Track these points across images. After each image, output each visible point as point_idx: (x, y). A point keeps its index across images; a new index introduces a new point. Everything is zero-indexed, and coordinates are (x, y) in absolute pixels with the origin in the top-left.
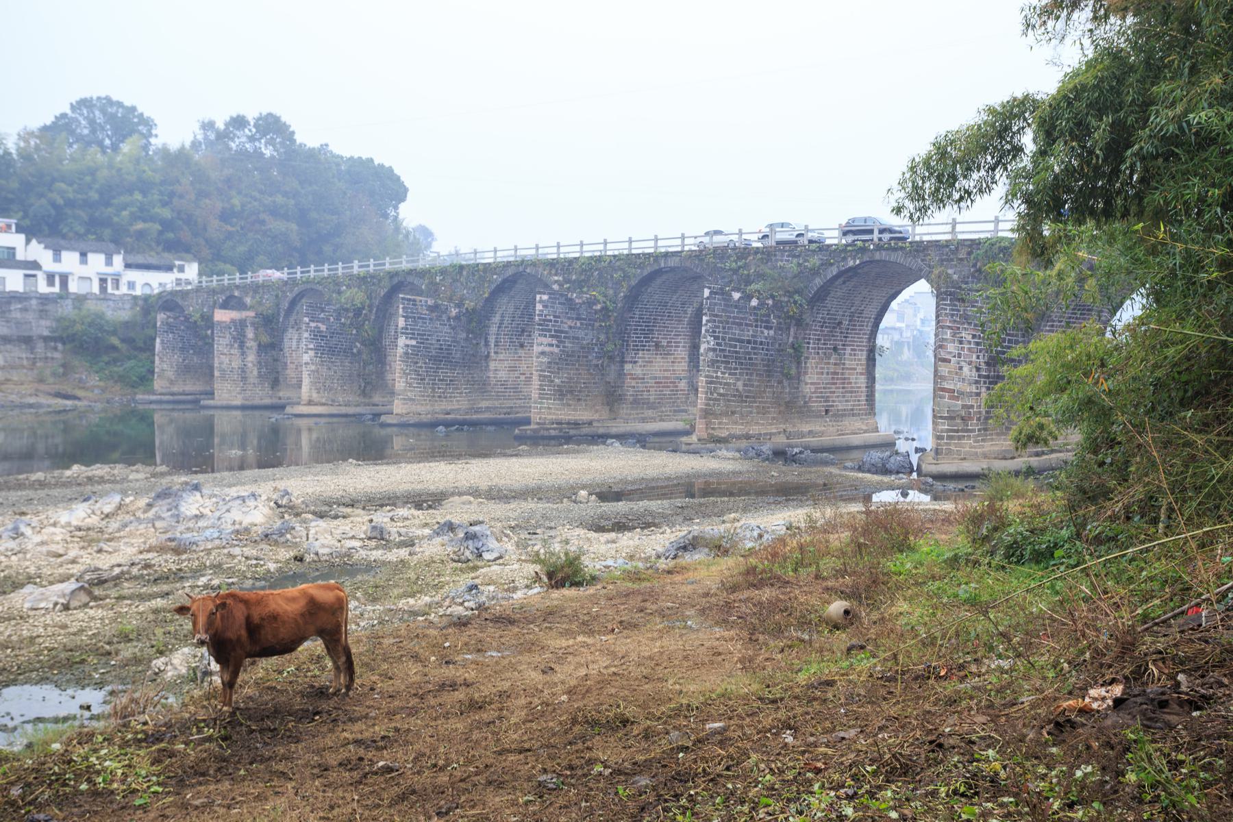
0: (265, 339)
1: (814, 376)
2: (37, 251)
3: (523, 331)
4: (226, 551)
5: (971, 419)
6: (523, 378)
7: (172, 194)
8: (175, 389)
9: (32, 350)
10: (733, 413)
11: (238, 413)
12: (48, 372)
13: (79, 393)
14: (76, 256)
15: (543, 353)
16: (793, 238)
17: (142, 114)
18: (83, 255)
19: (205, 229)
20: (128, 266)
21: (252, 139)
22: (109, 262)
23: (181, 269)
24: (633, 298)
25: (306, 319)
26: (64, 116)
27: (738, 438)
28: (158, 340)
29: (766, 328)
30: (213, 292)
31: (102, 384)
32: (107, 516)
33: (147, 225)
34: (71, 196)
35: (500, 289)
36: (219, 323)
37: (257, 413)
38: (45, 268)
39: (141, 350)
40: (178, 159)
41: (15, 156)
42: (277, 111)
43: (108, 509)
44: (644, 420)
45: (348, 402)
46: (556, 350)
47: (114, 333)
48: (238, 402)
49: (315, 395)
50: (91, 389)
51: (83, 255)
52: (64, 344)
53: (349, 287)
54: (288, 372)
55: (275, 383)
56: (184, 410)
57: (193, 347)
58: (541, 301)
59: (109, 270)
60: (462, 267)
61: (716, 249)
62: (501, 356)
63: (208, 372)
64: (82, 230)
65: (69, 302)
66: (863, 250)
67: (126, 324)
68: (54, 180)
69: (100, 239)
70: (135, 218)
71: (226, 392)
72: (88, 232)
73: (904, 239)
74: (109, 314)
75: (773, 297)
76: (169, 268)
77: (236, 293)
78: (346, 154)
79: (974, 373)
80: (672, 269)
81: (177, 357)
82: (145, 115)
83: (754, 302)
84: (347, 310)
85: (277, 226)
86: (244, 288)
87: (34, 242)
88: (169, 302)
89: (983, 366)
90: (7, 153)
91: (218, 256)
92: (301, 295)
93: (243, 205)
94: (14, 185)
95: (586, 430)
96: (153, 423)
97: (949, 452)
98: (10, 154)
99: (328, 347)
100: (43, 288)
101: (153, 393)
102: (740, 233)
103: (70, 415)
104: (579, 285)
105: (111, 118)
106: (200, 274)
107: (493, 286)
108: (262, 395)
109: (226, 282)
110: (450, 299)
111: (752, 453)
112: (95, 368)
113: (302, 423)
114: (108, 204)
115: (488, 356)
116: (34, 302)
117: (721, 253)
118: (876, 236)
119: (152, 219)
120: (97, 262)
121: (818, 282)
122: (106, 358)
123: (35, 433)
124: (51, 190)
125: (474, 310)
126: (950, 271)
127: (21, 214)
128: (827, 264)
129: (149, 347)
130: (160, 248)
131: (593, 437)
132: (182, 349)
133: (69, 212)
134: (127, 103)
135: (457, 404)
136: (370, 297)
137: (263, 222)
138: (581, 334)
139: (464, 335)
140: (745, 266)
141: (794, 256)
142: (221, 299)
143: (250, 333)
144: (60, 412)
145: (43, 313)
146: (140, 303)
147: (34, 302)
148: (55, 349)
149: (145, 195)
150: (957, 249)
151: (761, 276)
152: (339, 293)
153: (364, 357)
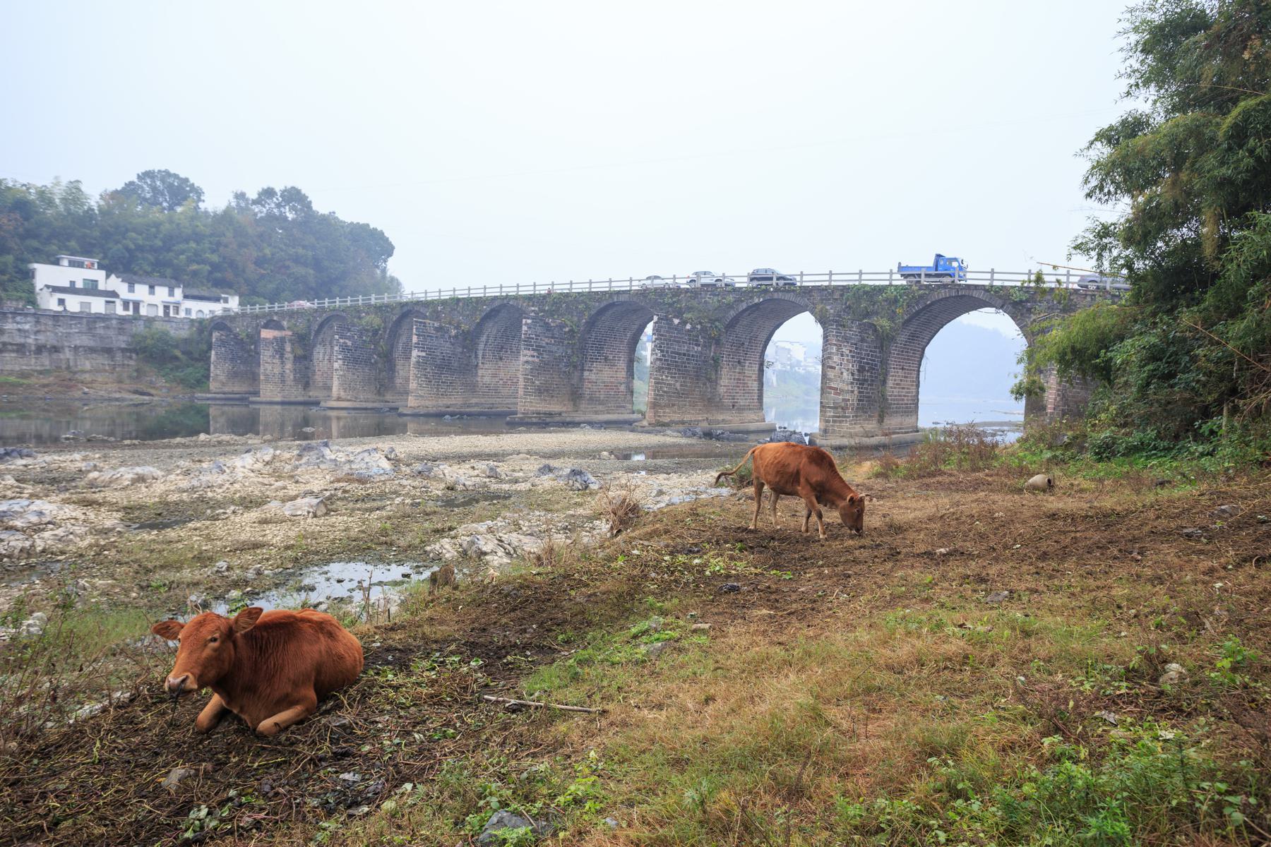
0: (300, 352)
1: (726, 380)
2: (115, 283)
3: (502, 348)
4: (397, 482)
5: (848, 409)
6: (501, 382)
7: (219, 244)
8: (226, 389)
9: (113, 358)
10: (673, 405)
11: (278, 407)
12: (125, 375)
13: (153, 391)
14: (146, 288)
15: (527, 362)
16: (713, 282)
17: (193, 184)
18: (152, 287)
19: (244, 271)
20: (186, 297)
21: (278, 206)
22: (171, 294)
23: (226, 301)
24: (592, 323)
25: (337, 337)
26: (132, 183)
27: (677, 423)
28: (213, 352)
29: (696, 345)
30: (257, 317)
31: (167, 385)
32: (267, 463)
33: (201, 266)
34: (141, 242)
35: (488, 317)
36: (265, 339)
37: (293, 408)
38: (122, 296)
39: (197, 360)
40: (225, 217)
41: (97, 212)
42: (299, 186)
43: (267, 458)
44: (596, 413)
45: (367, 398)
46: (536, 360)
47: (176, 347)
48: (278, 399)
49: (342, 394)
50: (160, 388)
51: (152, 287)
52: (137, 354)
53: (367, 313)
54: (316, 377)
55: (306, 386)
56: (232, 405)
57: (240, 358)
58: (526, 324)
59: (171, 299)
60: (459, 300)
61: (656, 289)
62: (486, 366)
63: (254, 378)
64: (149, 269)
65: (141, 323)
66: (766, 291)
67: (186, 341)
68: (127, 230)
69: (163, 276)
70: (190, 261)
71: (269, 392)
72: (153, 270)
73: (794, 284)
74: (172, 332)
75: (701, 323)
76: (217, 300)
77: (275, 318)
78: (348, 220)
79: (850, 377)
80: (622, 303)
81: (228, 366)
82: (196, 185)
83: (688, 327)
84: (367, 331)
85: (299, 270)
86: (282, 314)
87: (113, 276)
88: (219, 324)
89: (856, 372)
90: (91, 209)
91: (254, 292)
92: (328, 320)
93: (273, 255)
94: (97, 233)
95: (557, 419)
96: (208, 415)
97: (834, 431)
98: (93, 210)
99: (353, 358)
100: (120, 311)
101: (209, 392)
102: (675, 278)
103: (145, 408)
104: (551, 314)
105: (170, 187)
106: (240, 304)
107: (483, 314)
108: (296, 394)
109: (267, 310)
110: (450, 324)
111: (689, 433)
112: (162, 373)
113: (333, 414)
114: (169, 250)
115: (477, 366)
116: (114, 322)
117: (660, 292)
118: (774, 282)
119: (204, 262)
120: (162, 293)
121: (732, 313)
122: (170, 366)
123: (114, 422)
124: (124, 238)
125: (468, 331)
126: (828, 307)
127: (101, 255)
128: (739, 301)
129: (205, 358)
130: (210, 285)
131: (563, 423)
132: (232, 360)
133: (140, 255)
134: (182, 175)
135: (455, 400)
136: (385, 322)
137: (288, 267)
138: (554, 348)
139: (460, 350)
140: (678, 301)
141: (715, 295)
142: (263, 322)
143: (288, 348)
144: (136, 405)
145: (121, 331)
146: (196, 324)
147: (114, 322)
148: (130, 358)
149: (198, 243)
150: (833, 292)
151: (689, 309)
152: (360, 318)
153: (380, 365)
